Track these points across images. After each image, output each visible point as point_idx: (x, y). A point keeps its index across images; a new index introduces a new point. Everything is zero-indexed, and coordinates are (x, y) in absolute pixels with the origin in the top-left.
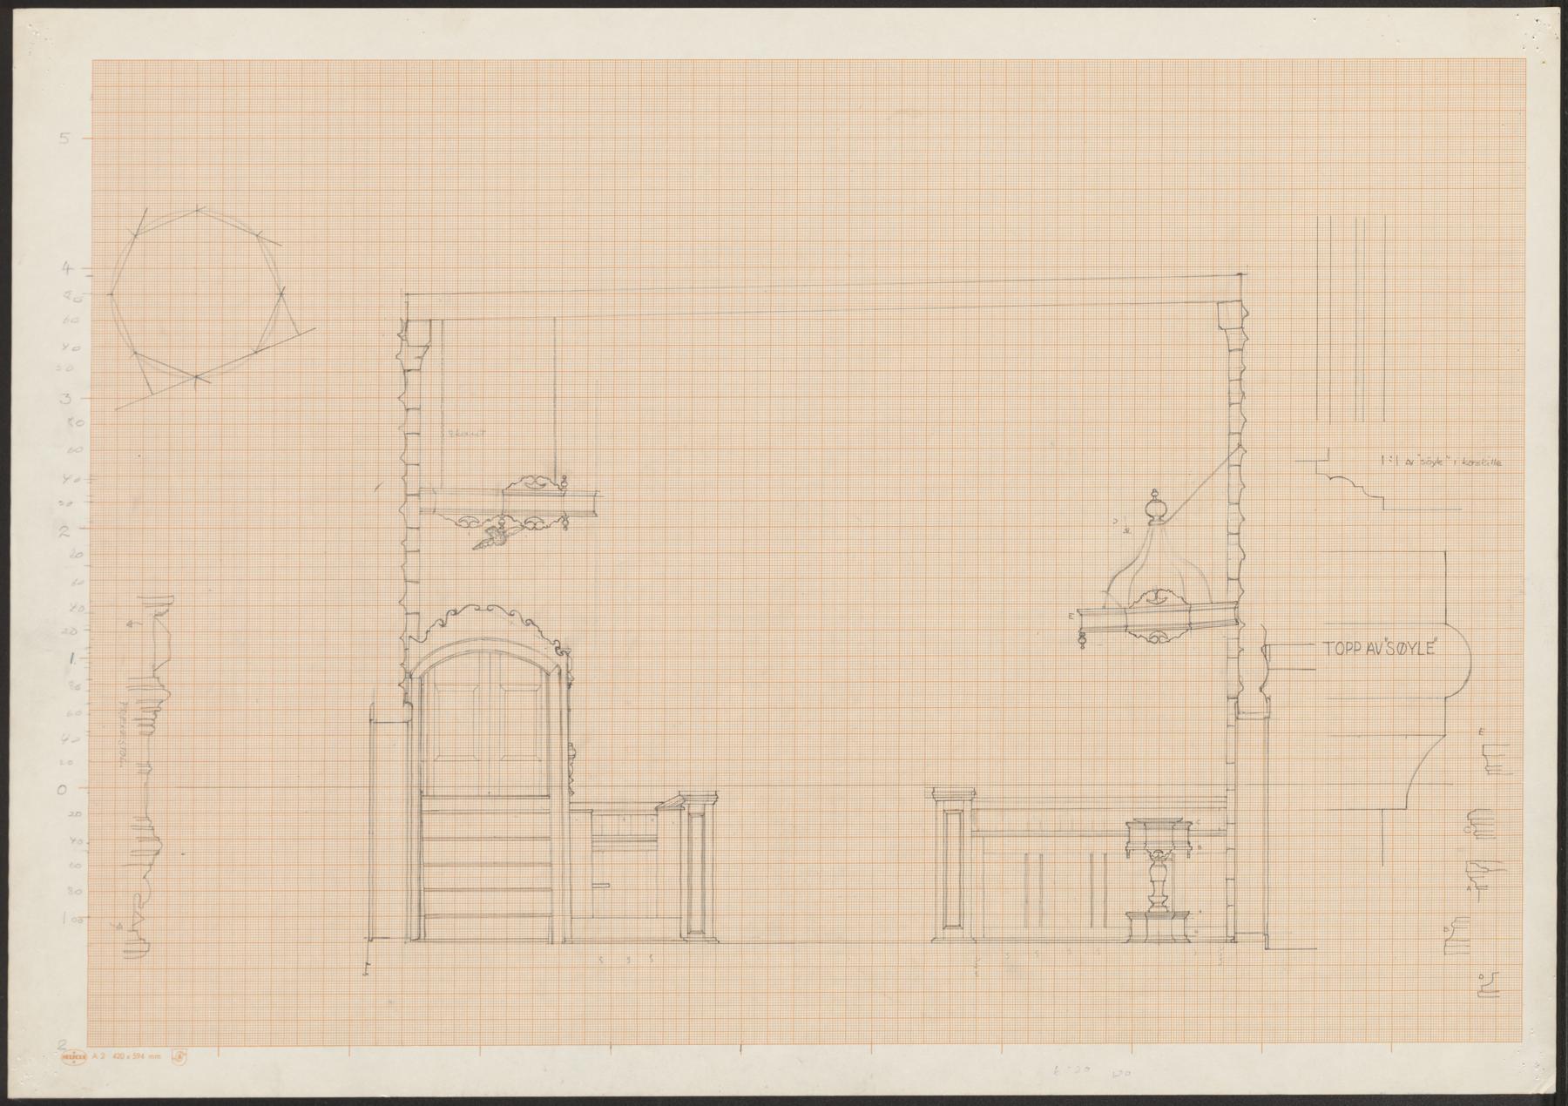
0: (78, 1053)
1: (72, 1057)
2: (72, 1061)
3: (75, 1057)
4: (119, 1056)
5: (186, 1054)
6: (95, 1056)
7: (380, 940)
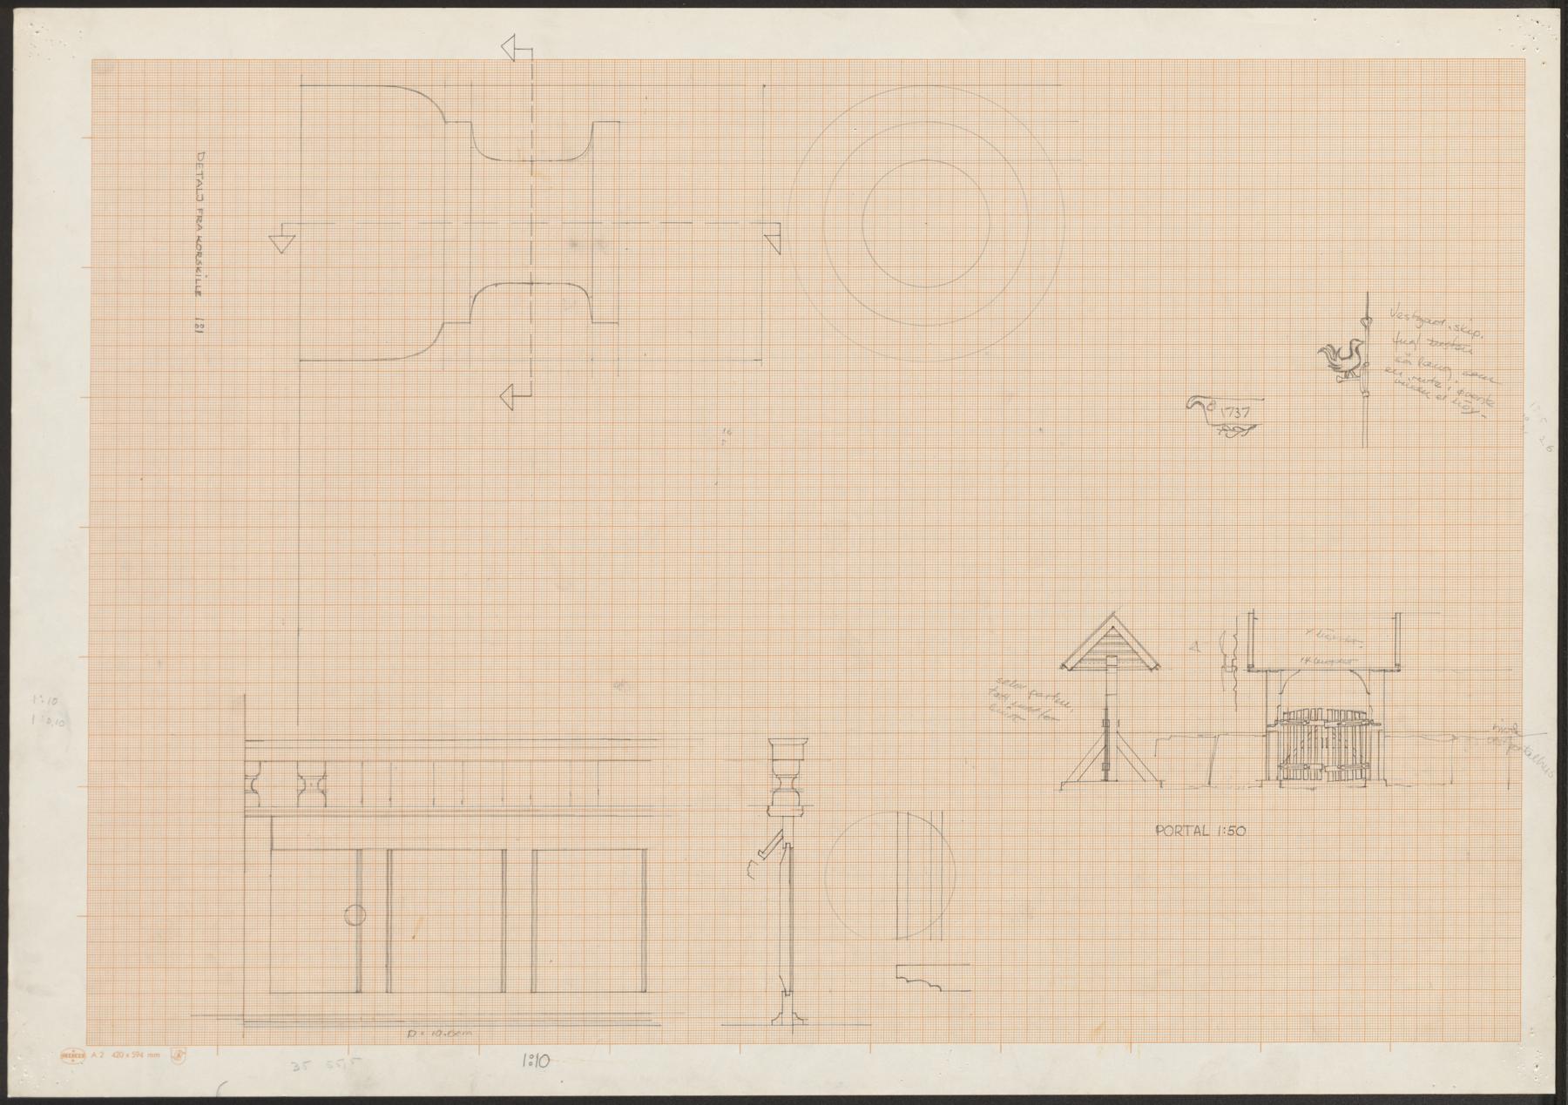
0: (78, 1052)
1: (70, 1056)
2: (76, 1052)
3: (74, 1056)
4: (117, 1055)
5: (185, 1053)
6: (94, 1055)
7: (1265, 710)
